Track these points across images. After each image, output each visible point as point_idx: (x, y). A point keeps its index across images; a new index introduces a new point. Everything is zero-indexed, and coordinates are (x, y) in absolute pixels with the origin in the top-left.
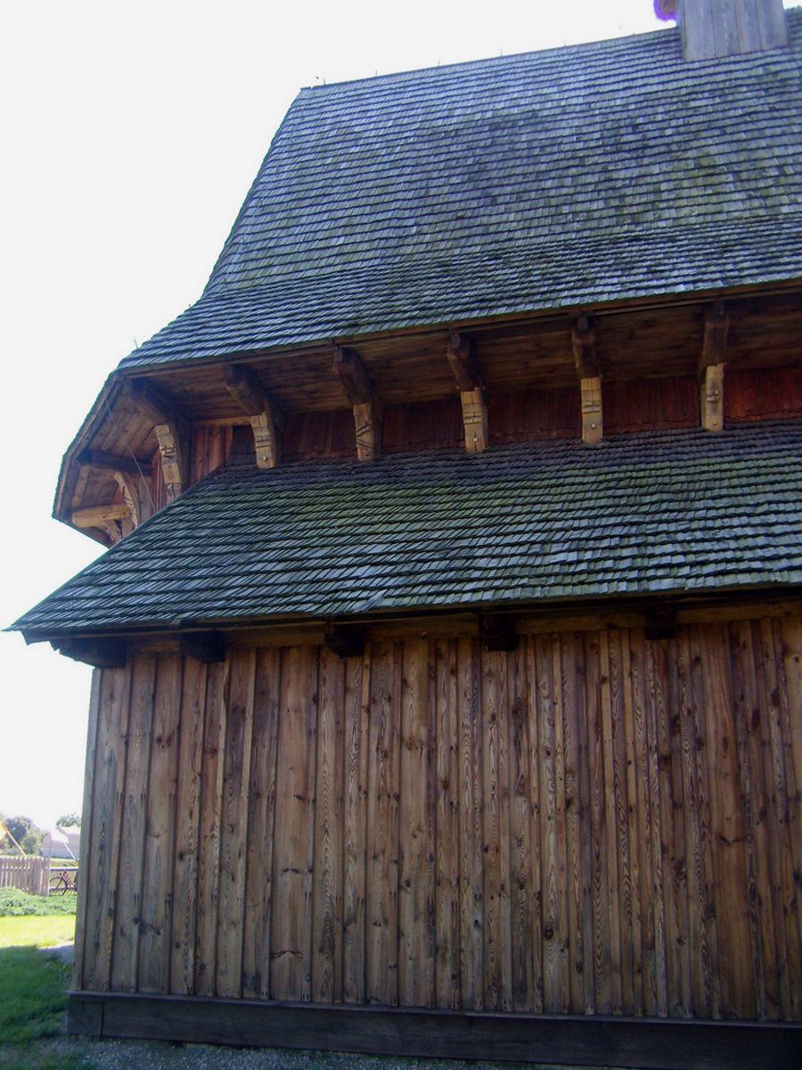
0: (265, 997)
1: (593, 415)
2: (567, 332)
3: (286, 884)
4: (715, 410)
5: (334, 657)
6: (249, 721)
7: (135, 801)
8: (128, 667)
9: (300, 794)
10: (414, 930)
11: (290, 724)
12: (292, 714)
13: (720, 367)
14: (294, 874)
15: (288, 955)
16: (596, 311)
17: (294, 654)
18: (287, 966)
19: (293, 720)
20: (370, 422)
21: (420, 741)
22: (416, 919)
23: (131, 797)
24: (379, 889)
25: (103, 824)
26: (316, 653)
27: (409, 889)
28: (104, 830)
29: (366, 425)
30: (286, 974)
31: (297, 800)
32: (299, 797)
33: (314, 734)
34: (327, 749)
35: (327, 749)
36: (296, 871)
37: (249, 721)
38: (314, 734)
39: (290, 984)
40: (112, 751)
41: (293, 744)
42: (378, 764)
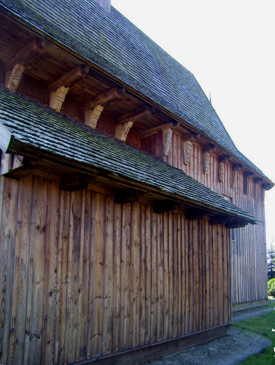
0: (88, 358)
1: (96, 119)
2: (109, 87)
3: (96, 304)
4: (125, 135)
5: (112, 202)
6: (83, 225)
7: (24, 262)
8: (162, 213)
9: (102, 262)
10: (136, 317)
11: (97, 229)
12: (98, 224)
13: (132, 123)
14: (99, 298)
15: (97, 336)
16: (130, 90)
17: (98, 195)
18: (96, 341)
19: (98, 227)
20: (21, 76)
21: (138, 243)
22: (136, 313)
23: (22, 260)
24: (126, 302)
25: (5, 276)
26: (105, 199)
27: (135, 301)
28: (5, 279)
29: (19, 76)
30: (96, 345)
31: (100, 265)
32: (101, 264)
33: (105, 235)
34: (110, 242)
35: (110, 242)
36: (100, 297)
37: (83, 225)
38: (105, 235)
39: (97, 349)
40: (10, 231)
41: (98, 239)
42: (126, 251)
